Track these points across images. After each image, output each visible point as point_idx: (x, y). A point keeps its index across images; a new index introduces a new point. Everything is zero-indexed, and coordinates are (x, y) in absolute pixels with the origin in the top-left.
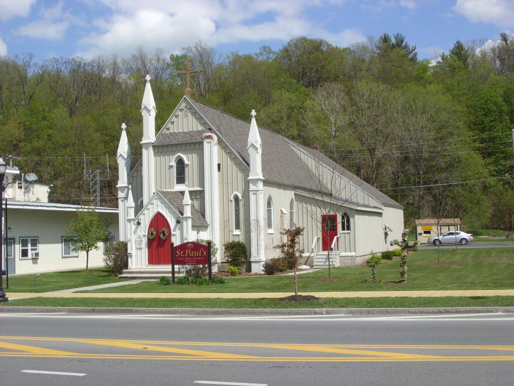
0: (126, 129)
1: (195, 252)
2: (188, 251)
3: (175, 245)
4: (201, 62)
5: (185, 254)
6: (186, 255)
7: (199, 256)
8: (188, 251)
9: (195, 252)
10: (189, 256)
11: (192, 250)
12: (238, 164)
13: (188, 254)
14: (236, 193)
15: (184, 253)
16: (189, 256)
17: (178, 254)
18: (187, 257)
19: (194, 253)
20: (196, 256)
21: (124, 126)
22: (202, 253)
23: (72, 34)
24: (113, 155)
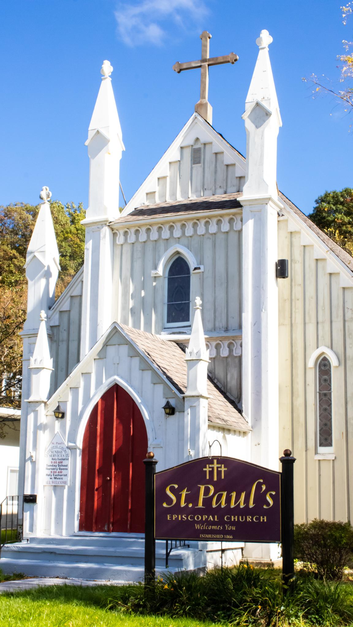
0: (113, 76)
1: (234, 494)
2: (207, 491)
3: (159, 468)
4: (151, 614)
5: (196, 502)
6: (200, 505)
7: (246, 511)
8: (207, 491)
9: (234, 494)
10: (208, 508)
11: (220, 486)
12: (349, 253)
13: (208, 502)
14: (324, 349)
15: (193, 498)
16: (208, 508)
17: (170, 501)
18: (201, 512)
19: (217, 528)
20: (237, 511)
21: (107, 67)
22: (260, 498)
23: (79, 449)
24: (52, 327)
